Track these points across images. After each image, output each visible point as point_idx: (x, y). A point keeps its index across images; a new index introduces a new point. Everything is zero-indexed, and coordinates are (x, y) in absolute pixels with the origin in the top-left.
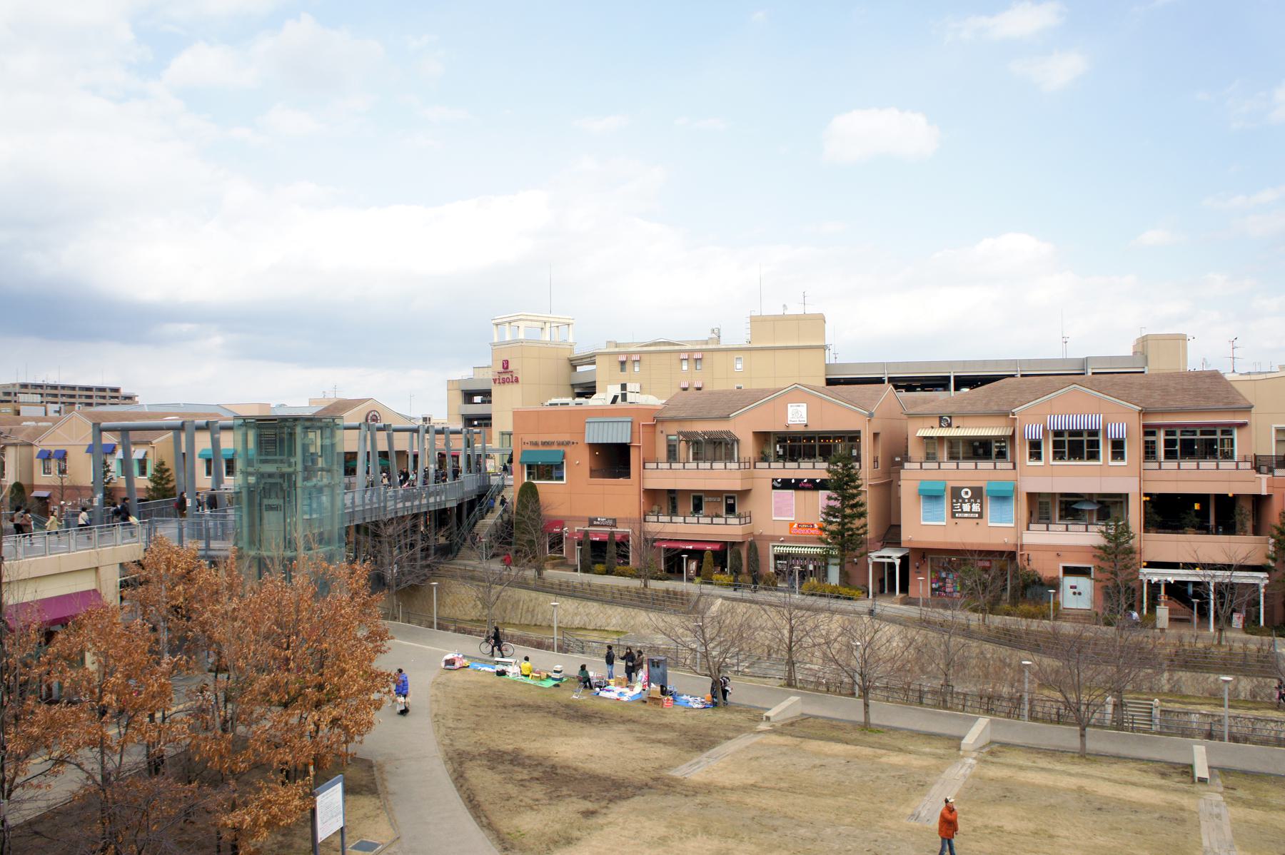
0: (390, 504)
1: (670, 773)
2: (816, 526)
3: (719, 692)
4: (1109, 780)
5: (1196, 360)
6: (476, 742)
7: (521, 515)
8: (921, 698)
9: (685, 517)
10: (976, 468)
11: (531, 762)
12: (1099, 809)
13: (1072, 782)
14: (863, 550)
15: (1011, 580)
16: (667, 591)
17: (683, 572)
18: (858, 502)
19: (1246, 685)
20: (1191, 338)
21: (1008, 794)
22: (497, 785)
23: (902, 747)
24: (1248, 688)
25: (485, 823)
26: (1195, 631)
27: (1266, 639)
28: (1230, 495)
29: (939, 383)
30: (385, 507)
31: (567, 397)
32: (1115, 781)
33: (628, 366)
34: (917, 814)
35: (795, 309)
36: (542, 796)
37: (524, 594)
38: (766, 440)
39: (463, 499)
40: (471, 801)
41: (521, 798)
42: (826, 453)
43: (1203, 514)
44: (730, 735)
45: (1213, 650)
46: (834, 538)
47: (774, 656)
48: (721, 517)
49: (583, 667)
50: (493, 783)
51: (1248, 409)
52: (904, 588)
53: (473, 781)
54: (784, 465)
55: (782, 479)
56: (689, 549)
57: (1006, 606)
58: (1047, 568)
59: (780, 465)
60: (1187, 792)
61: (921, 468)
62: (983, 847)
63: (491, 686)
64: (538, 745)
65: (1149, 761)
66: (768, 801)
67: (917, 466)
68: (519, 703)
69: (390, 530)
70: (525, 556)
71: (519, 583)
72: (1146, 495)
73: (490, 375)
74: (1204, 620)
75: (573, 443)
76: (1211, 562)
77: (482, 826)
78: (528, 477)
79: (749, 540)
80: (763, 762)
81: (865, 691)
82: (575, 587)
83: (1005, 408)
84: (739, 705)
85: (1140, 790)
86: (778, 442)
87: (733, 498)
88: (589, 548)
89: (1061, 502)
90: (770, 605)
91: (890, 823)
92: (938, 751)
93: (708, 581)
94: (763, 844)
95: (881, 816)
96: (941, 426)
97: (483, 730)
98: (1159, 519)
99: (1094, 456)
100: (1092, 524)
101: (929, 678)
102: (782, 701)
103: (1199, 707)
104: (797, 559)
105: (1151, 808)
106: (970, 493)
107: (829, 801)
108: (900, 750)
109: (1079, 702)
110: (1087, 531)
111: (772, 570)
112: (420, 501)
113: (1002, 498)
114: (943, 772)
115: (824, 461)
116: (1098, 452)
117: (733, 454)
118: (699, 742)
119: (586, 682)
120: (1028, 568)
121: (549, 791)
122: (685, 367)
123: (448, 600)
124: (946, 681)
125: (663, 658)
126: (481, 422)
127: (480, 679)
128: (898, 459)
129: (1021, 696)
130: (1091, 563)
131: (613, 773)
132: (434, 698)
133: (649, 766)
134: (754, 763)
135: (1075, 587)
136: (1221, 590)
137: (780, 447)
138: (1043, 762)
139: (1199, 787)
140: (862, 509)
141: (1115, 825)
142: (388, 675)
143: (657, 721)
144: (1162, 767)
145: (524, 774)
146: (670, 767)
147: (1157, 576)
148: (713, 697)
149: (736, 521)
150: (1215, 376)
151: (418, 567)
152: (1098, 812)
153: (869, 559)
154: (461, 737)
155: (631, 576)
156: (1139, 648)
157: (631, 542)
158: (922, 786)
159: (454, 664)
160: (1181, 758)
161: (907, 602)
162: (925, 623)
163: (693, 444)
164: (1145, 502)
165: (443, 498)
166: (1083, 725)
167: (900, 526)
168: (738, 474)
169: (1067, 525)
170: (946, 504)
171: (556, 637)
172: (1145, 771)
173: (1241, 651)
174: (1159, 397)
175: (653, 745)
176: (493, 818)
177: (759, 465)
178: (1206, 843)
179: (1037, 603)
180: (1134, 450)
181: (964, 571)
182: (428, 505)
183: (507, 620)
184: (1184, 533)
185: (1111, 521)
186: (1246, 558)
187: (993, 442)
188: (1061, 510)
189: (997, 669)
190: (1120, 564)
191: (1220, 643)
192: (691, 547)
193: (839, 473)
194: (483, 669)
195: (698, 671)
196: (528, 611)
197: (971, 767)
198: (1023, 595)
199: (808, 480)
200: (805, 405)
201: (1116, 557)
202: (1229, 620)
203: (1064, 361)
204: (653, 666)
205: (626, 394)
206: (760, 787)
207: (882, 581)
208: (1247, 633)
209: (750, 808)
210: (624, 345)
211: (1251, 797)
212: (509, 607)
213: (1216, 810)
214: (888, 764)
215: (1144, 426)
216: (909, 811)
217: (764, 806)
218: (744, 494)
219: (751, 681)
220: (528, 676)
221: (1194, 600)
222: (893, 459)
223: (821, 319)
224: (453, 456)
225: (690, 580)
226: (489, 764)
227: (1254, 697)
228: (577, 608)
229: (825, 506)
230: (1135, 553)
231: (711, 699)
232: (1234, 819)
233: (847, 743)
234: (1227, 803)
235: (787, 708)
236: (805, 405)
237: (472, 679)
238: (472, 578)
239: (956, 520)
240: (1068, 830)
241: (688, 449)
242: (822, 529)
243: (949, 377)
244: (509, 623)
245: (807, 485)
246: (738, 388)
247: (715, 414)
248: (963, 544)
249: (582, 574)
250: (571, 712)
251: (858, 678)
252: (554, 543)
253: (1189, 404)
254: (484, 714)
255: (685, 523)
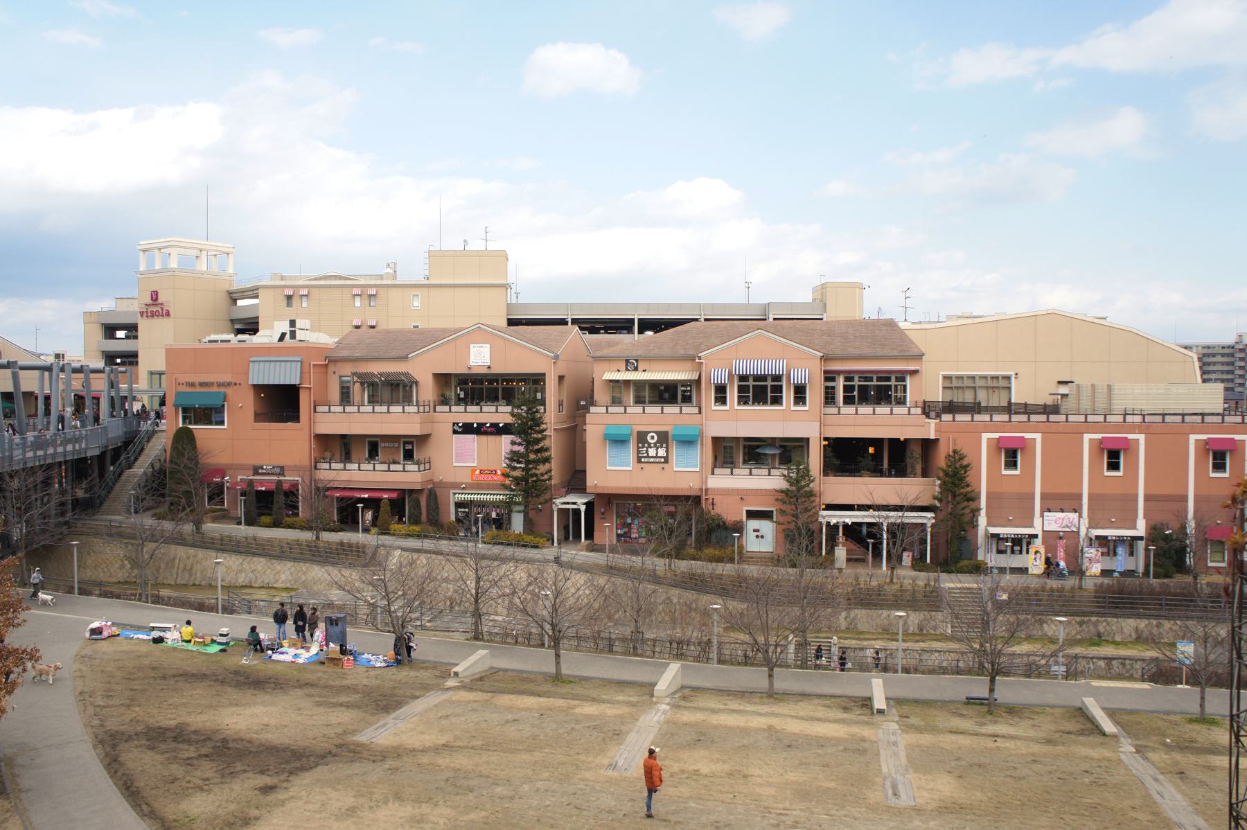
0: (18, 454)
1: (354, 738)
2: (499, 472)
3: (403, 650)
4: (797, 717)
5: (872, 307)
6: (131, 720)
7: (176, 464)
8: (611, 646)
9: (359, 464)
10: (662, 412)
11: (198, 737)
12: (789, 746)
13: (762, 722)
14: (547, 496)
15: (696, 524)
16: (342, 544)
17: (358, 523)
18: (542, 447)
19: (915, 618)
20: (867, 287)
21: (702, 738)
22: (160, 767)
23: (596, 697)
24: (916, 622)
25: (146, 813)
26: (870, 570)
27: (932, 575)
28: (902, 439)
29: (623, 326)
30: (11, 457)
31: (228, 333)
32: (802, 718)
33: (295, 301)
34: (614, 763)
35: (476, 245)
36: (214, 774)
37: (181, 551)
38: (446, 382)
39: (107, 447)
40: (128, 788)
41: (188, 778)
42: (509, 397)
43: (877, 457)
44: (417, 693)
45: (885, 587)
46: (518, 484)
47: (457, 608)
48: (399, 463)
49: (253, 629)
50: (154, 765)
51: (919, 357)
52: (590, 535)
53: (130, 764)
54: (466, 409)
55: (464, 424)
56: (364, 498)
57: (692, 551)
58: (731, 512)
59: (461, 408)
60: (867, 723)
61: (607, 412)
62: (680, 792)
63: (147, 656)
64: (204, 717)
65: (832, 696)
66: (461, 761)
67: (603, 410)
68: (181, 672)
69: (15, 484)
70: (184, 509)
71: (175, 539)
72: (826, 439)
73: (135, 307)
74: (878, 559)
75: (235, 384)
76: (885, 503)
77: (143, 815)
78: (184, 422)
79: (429, 487)
80: (454, 720)
81: (556, 641)
82: (239, 542)
83: (692, 352)
84: (424, 662)
85: (826, 724)
86: (459, 384)
87: (412, 443)
88: (253, 498)
89: (745, 447)
90: (456, 555)
91: (588, 775)
92: (632, 699)
93: (385, 531)
94: (458, 807)
95: (578, 768)
96: (627, 370)
97: (139, 706)
98: (837, 462)
99: (777, 401)
100: (774, 468)
101: (615, 625)
102: (470, 655)
103: (873, 642)
104: (483, 506)
105: (836, 742)
106: (649, 439)
107: (524, 757)
108: (594, 700)
109: (767, 644)
110: (751, 474)
111: (453, 518)
112: (55, 450)
113: (687, 442)
114: (637, 720)
115: (508, 405)
116: (781, 397)
117: (411, 396)
118: (385, 702)
119: (255, 644)
120: (713, 513)
121: (221, 767)
122: (358, 304)
123: (89, 562)
124: (637, 627)
125: (342, 615)
126: (125, 360)
127: (136, 648)
128: (583, 403)
129: (709, 639)
130: (773, 505)
131: (292, 742)
132: (78, 674)
133: (330, 732)
134: (444, 722)
135: (758, 531)
136: (894, 530)
137: (461, 390)
138: (734, 704)
139: (878, 718)
140: (547, 454)
141: (804, 761)
142: (23, 652)
143: (337, 683)
144: (844, 701)
145: (190, 752)
146: (354, 732)
147: (836, 518)
148: (396, 654)
149: (415, 468)
150: (891, 324)
151: (52, 526)
152: (788, 749)
153: (554, 505)
154: (112, 716)
155: (302, 528)
156: (819, 587)
157: (300, 492)
158: (618, 735)
159: (101, 633)
160: (860, 692)
161: (592, 549)
162: (610, 570)
163: (368, 386)
164: (824, 446)
165: (83, 445)
166: (770, 665)
167: (585, 471)
168: (417, 418)
169: (751, 469)
170: (631, 451)
171: (220, 597)
172: (828, 707)
173: (910, 587)
174: (839, 344)
175: (335, 709)
176: (156, 805)
177: (439, 408)
178: (884, 769)
179: (722, 547)
180: (815, 395)
181: (649, 517)
182: (65, 453)
183: (160, 580)
184: (860, 476)
185: (793, 465)
186: (917, 498)
187: (679, 386)
188: (744, 454)
189: (683, 614)
190: (800, 508)
191: (891, 580)
192: (366, 496)
193: (523, 417)
194: (136, 637)
195: (379, 627)
196: (185, 569)
197: (664, 712)
198: (708, 540)
199: (491, 424)
200: (488, 345)
201: (797, 500)
202: (900, 559)
203: (747, 306)
204: (332, 624)
205: (295, 331)
206: (453, 747)
207: (566, 528)
208: (915, 570)
209: (443, 770)
210: (290, 278)
211: (922, 723)
212: (163, 566)
213: (893, 738)
214: (582, 714)
215: (826, 372)
216: (606, 761)
217: (458, 767)
218: (423, 439)
219: (435, 636)
220: (190, 641)
221: (869, 540)
222: (578, 402)
223: (503, 256)
224: (94, 398)
225: (366, 530)
226: (148, 743)
227: (921, 630)
228: (242, 564)
229: (508, 451)
230: (815, 496)
231: (394, 656)
232: (909, 745)
233: (540, 696)
234: (902, 730)
235: (476, 662)
236: (488, 345)
237: (124, 648)
238: (121, 535)
239: (643, 465)
240: (760, 768)
241: (364, 391)
242: (505, 475)
243: (633, 320)
244: (163, 584)
245: (490, 430)
246: (414, 327)
247: (393, 354)
248: (650, 489)
249: (247, 527)
250: (241, 679)
251: (547, 627)
252: (214, 494)
253: (867, 351)
254: (139, 687)
255: (359, 470)
